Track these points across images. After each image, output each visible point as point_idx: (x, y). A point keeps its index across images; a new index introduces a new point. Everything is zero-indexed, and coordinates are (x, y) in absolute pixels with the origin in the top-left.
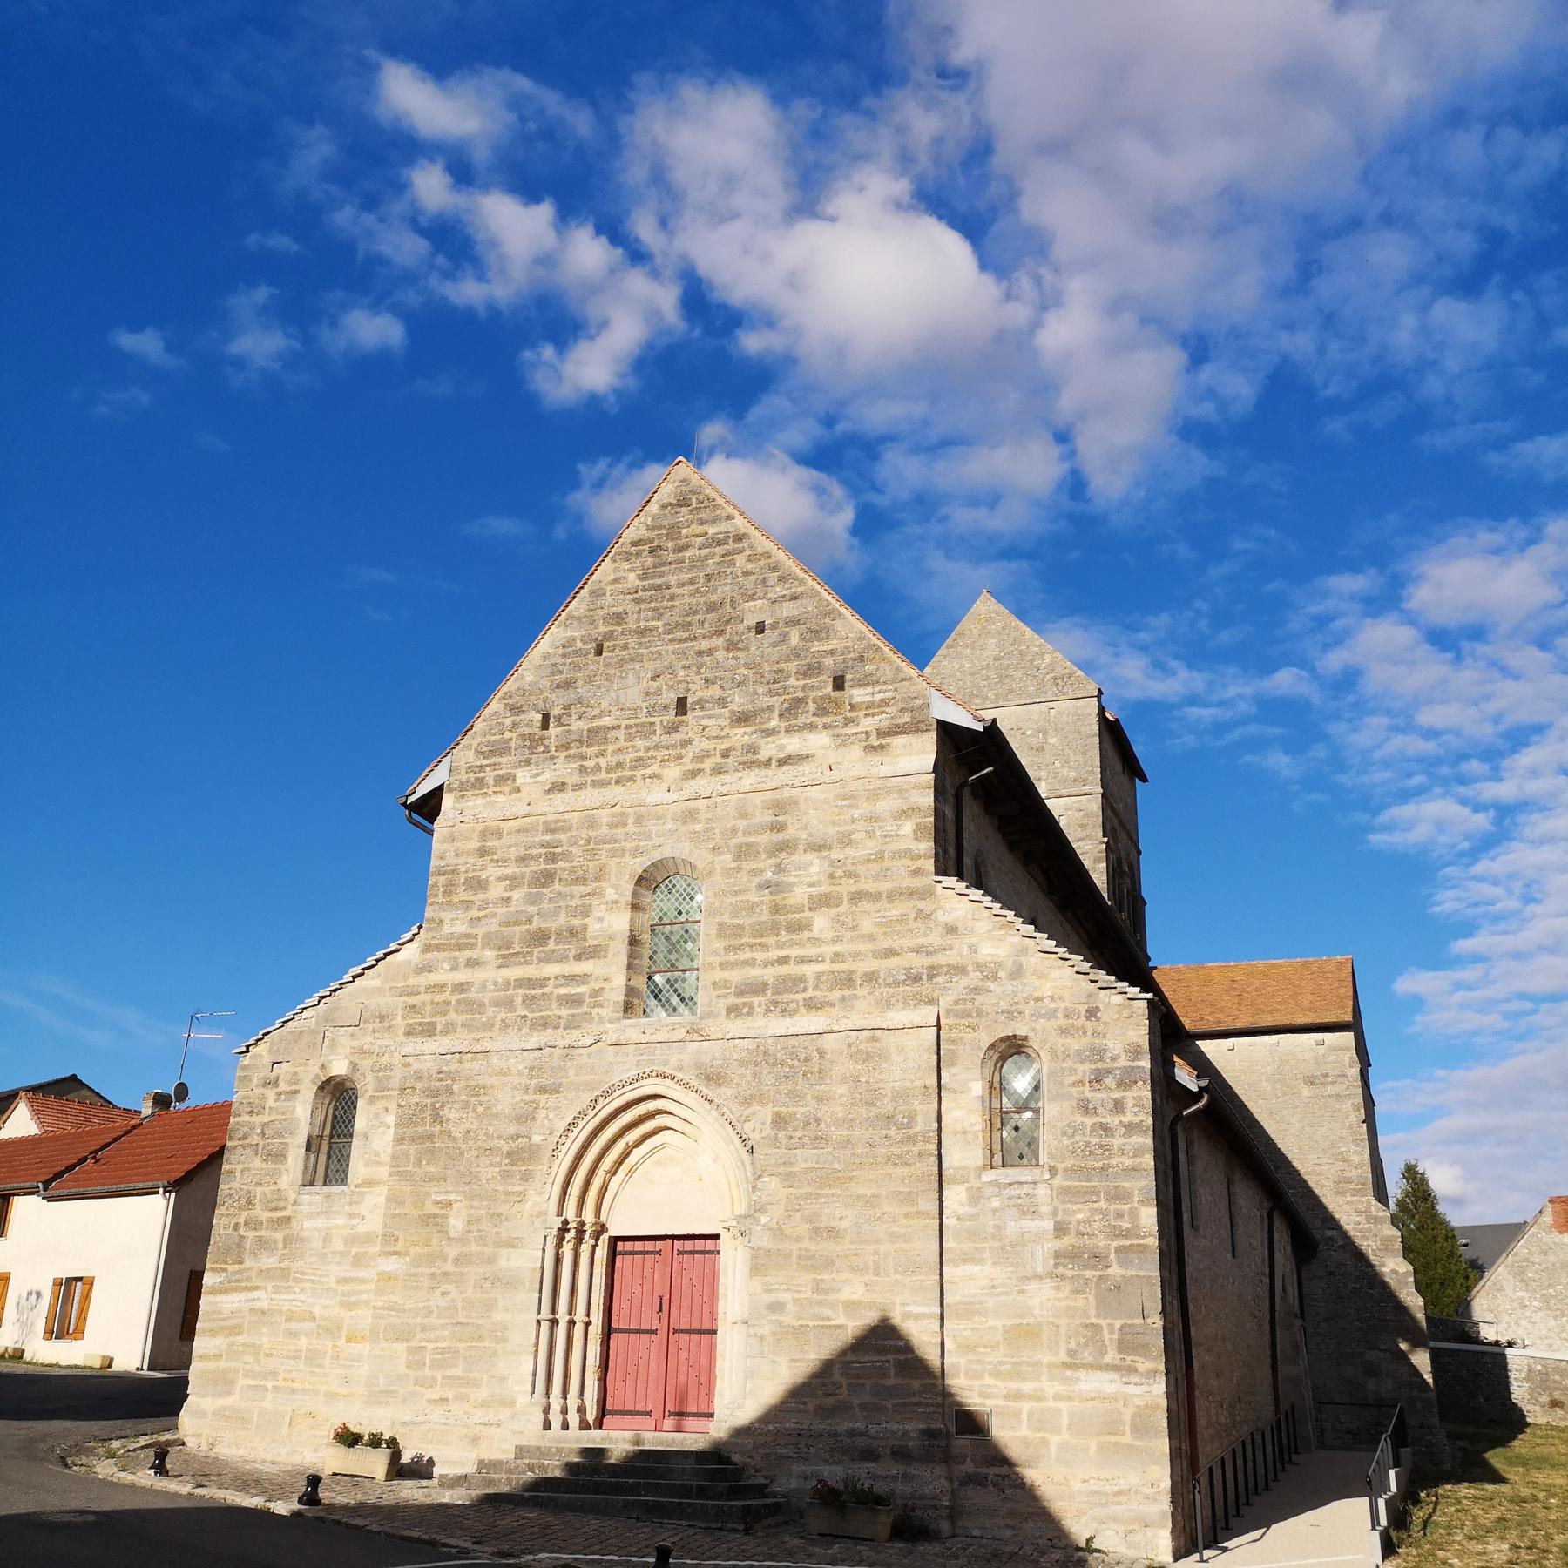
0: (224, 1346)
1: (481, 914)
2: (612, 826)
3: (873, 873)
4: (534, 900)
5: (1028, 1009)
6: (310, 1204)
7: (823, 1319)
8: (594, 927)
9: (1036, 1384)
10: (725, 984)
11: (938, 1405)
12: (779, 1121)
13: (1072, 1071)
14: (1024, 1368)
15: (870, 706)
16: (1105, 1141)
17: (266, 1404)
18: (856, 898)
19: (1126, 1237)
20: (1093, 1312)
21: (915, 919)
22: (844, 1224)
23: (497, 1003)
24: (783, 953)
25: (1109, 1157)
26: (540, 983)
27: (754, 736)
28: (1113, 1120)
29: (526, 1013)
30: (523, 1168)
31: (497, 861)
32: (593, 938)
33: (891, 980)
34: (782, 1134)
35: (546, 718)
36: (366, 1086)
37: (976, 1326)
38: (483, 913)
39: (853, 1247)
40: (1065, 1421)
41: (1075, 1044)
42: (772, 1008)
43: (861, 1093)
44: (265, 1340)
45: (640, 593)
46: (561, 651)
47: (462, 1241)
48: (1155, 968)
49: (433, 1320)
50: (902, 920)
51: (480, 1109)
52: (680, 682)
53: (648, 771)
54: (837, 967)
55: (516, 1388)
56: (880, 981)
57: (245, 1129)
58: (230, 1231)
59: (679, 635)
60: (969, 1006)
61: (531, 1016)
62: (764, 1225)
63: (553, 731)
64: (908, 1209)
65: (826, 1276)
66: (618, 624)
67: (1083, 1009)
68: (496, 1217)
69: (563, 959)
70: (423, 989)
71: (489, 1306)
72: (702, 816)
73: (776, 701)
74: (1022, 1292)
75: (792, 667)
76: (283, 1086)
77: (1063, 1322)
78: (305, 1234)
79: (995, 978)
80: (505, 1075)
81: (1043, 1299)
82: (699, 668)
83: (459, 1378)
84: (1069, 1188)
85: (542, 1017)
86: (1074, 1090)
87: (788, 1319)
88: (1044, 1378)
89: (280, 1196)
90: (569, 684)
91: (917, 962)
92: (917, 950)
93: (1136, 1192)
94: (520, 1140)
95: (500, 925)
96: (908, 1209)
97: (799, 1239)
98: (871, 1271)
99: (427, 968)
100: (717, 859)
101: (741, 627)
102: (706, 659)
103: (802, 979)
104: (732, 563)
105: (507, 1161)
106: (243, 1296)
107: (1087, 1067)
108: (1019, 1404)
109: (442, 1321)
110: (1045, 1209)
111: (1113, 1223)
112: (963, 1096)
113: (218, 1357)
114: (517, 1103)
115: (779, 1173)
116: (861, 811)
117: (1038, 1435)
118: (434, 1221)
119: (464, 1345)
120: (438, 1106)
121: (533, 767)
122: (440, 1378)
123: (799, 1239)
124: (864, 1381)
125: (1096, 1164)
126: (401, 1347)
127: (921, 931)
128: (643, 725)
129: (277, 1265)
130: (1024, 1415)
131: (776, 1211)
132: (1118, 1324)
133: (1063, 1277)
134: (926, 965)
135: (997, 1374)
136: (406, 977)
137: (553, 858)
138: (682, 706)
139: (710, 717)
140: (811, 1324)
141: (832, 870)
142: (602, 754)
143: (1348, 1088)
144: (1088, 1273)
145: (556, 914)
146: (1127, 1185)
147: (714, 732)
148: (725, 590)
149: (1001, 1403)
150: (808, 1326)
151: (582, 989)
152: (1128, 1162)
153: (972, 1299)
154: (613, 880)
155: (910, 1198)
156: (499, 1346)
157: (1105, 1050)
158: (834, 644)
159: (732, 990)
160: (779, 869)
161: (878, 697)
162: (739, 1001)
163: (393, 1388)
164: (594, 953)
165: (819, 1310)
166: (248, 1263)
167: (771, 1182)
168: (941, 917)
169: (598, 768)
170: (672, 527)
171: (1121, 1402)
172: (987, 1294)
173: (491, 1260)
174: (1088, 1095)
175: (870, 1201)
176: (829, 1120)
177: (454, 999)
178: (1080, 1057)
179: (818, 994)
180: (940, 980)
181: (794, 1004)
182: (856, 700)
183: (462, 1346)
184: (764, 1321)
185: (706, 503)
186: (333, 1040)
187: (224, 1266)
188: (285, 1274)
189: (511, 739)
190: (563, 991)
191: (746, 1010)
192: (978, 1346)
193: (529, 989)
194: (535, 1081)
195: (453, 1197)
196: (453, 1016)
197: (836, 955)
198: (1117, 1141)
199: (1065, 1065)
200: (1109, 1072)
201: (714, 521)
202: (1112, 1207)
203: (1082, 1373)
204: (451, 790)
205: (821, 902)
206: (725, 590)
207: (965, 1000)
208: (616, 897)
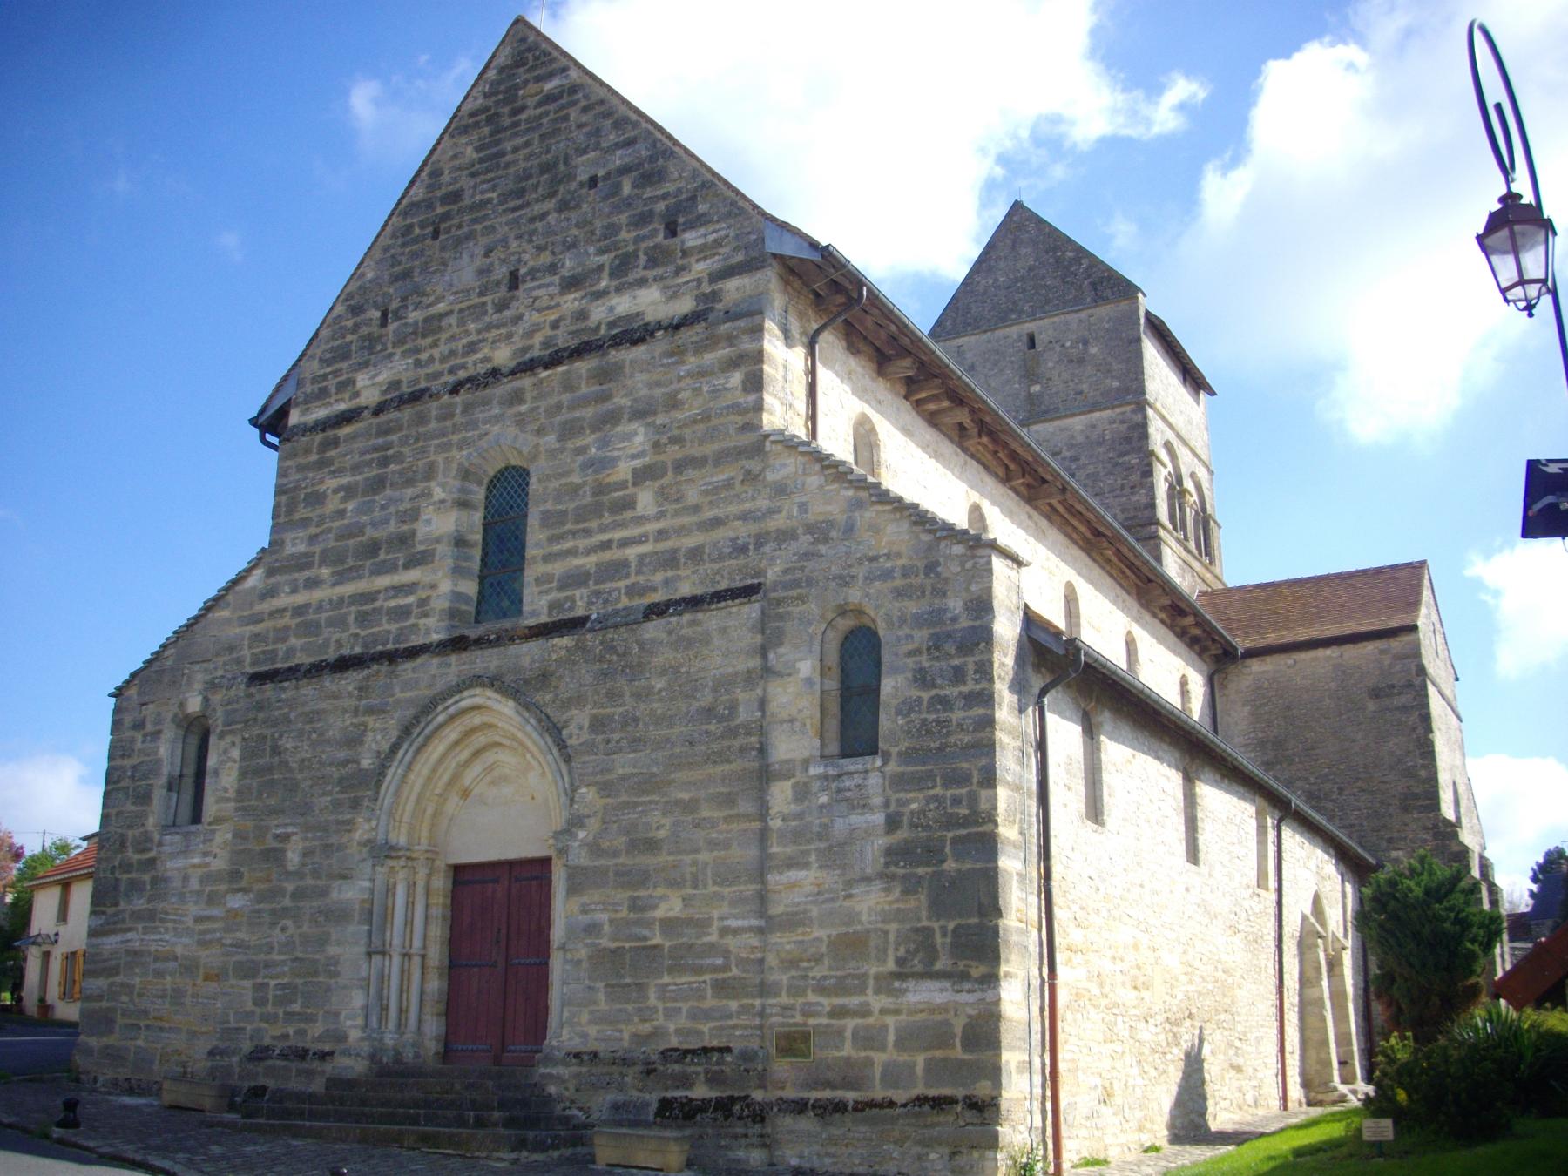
0: (105, 987)
1: (318, 530)
2: (441, 419)
3: (699, 435)
4: (365, 509)
5: (860, 572)
6: (172, 844)
7: (639, 939)
8: (422, 530)
9: (862, 999)
10: (549, 578)
11: (755, 1027)
12: (598, 724)
13: (909, 637)
14: (849, 981)
15: (702, 248)
16: (943, 716)
17: (140, 1042)
18: (680, 466)
19: (963, 826)
20: (924, 913)
21: (743, 481)
22: (662, 834)
23: (331, 623)
24: (605, 537)
25: (948, 735)
26: (370, 597)
27: (584, 301)
28: (951, 691)
29: (358, 631)
31: (334, 472)
32: (421, 543)
33: (716, 554)
34: (599, 738)
35: (385, 315)
36: (218, 721)
37: (800, 938)
38: (321, 529)
39: (671, 858)
40: (891, 1038)
41: (912, 607)
43: (680, 686)
44: (137, 980)
45: (477, 166)
46: (400, 241)
47: (299, 874)
49: (276, 957)
50: (729, 484)
51: (314, 736)
52: (513, 254)
53: (479, 356)
54: (661, 546)
55: (349, 1023)
56: (706, 557)
57: (118, 773)
58: (108, 875)
59: (511, 204)
60: (798, 574)
61: (363, 633)
63: (392, 326)
64: (726, 813)
65: (642, 893)
66: (455, 202)
67: (921, 565)
68: (328, 849)
69: (392, 568)
70: (266, 616)
71: (323, 941)
72: (528, 396)
73: (605, 259)
74: (850, 896)
75: (623, 218)
76: (149, 727)
77: (893, 927)
78: (169, 874)
79: (826, 540)
80: (336, 698)
81: (871, 903)
82: (531, 234)
83: (299, 1014)
84: (903, 774)
85: (373, 634)
86: (910, 662)
87: (605, 942)
88: (870, 991)
89: (147, 838)
90: (406, 275)
91: (743, 531)
92: (745, 517)
93: (975, 773)
95: (336, 540)
96: (726, 813)
97: (616, 854)
98: (688, 883)
99: (271, 593)
100: (542, 442)
101: (573, 186)
102: (538, 224)
103: (625, 564)
104: (566, 118)
106: (119, 938)
107: (925, 633)
108: (842, 1022)
109: (283, 957)
110: (877, 800)
111: (949, 811)
112: (791, 679)
113: (100, 998)
115: (597, 783)
116: (688, 367)
117: (863, 1054)
118: (274, 856)
119: (301, 981)
120: (277, 735)
121: (371, 368)
122: (281, 1015)
123: (616, 854)
124: (677, 1005)
125: (932, 745)
126: (248, 983)
127: (750, 494)
128: (474, 306)
129: (145, 906)
130: (848, 1034)
131: (594, 824)
132: (951, 926)
133: (893, 877)
134: (753, 533)
135: (821, 990)
136: (251, 605)
137: (384, 462)
138: (514, 281)
139: (539, 287)
141: (657, 437)
142: (435, 344)
143: (1415, 699)
144: (920, 871)
145: (386, 522)
146: (965, 765)
147: (545, 302)
148: (559, 146)
149: (825, 1021)
150: (624, 948)
151: (411, 599)
152: (967, 738)
153: (795, 909)
154: (441, 478)
155: (729, 800)
157: (945, 611)
158: (669, 187)
160: (604, 443)
161: (711, 238)
163: (242, 1025)
164: (421, 559)
165: (636, 930)
166: (122, 905)
168: (771, 476)
169: (431, 359)
170: (509, 90)
171: (952, 1013)
172: (811, 902)
173: (324, 893)
174: (926, 664)
175: (690, 806)
177: (294, 623)
178: (919, 621)
179: (641, 579)
180: (767, 549)
182: (690, 244)
183: (299, 981)
184: (581, 945)
185: (543, 59)
186: (189, 677)
187: (103, 909)
188: (151, 916)
189: (352, 342)
190: (392, 603)
192: (801, 960)
193: (361, 605)
195: (290, 829)
196: (293, 641)
197: (660, 532)
198: (957, 715)
199: (901, 633)
200: (949, 635)
201: (551, 75)
202: (949, 793)
203: (911, 984)
204: (297, 405)
205: (642, 476)
206: (559, 146)
207: (794, 568)
208: (443, 496)
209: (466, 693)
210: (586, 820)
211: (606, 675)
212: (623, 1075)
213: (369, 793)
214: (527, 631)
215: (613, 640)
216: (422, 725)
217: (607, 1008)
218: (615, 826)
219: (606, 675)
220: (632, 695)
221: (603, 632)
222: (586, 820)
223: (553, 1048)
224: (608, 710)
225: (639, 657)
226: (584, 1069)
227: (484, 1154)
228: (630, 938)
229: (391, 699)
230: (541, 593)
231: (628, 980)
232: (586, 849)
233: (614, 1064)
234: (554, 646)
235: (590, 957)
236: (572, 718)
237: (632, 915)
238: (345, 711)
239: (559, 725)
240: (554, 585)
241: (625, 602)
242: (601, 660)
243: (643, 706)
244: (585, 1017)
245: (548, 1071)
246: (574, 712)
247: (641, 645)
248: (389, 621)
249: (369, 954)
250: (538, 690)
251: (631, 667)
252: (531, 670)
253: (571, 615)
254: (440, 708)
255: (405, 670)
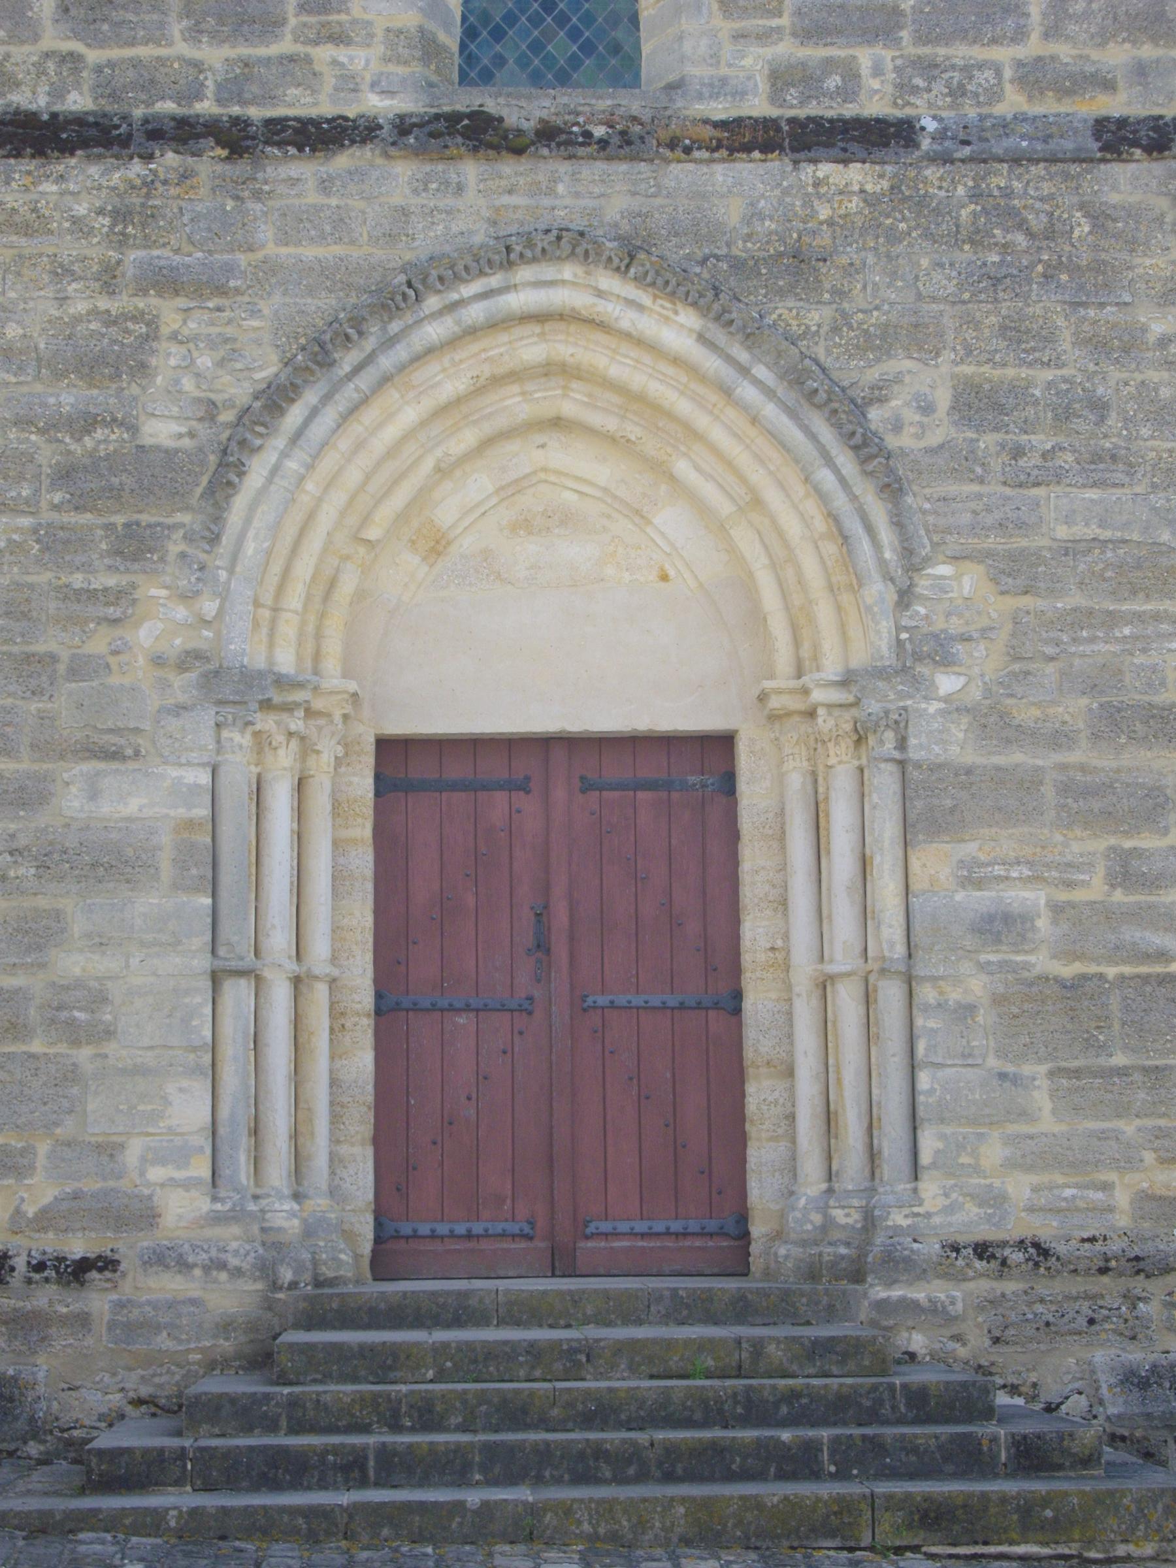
29: (77, 46)
30: (119, 520)
42: (919, 82)
48: (313, 776)
61: (93, 56)
62: (947, 699)
80: (27, 230)
85: (136, 63)
87: (1042, 962)
94: (99, 434)
97: (1060, 739)
105: (57, 497)
114: (77, 319)
115: (989, 554)
123: (1060, 739)
140: (1111, 972)
150: (1101, 977)
156: (84, 1054)
159: (785, 21)
162: (815, 53)
165: (1132, 934)
167: (958, 577)
176: (1131, 407)
181: (989, 74)
184: (966, 967)
191: (833, 81)
194: (133, 255)
209: (525, 273)
210: (959, 648)
211: (996, 281)
212: (1133, 1301)
213: (185, 518)
214: (708, 132)
215: (1008, 193)
216: (370, 344)
217: (1059, 1128)
218: (1050, 668)
219: (996, 281)
220: (1081, 341)
221: (970, 170)
222: (959, 648)
223: (897, 1230)
224: (1010, 372)
225: (1096, 248)
226: (1011, 1287)
227: (1149, 1549)
228: (1119, 954)
229: (242, 259)
230: (740, 36)
231: (1120, 1059)
232: (965, 720)
233: (1103, 1271)
234: (817, 184)
235: (998, 1000)
236: (898, 379)
237: (1118, 896)
238: (62, 272)
239: (858, 394)
240: (785, 21)
241: (1013, 101)
242: (977, 238)
243: (1115, 374)
244: (993, 1152)
245: (896, 1293)
246: (901, 364)
247: (1100, 218)
248: (194, 34)
249: (216, 979)
250: (782, 293)
251: (1075, 270)
252: (749, 237)
253: (849, 111)
254: (432, 302)
255: (294, 182)
